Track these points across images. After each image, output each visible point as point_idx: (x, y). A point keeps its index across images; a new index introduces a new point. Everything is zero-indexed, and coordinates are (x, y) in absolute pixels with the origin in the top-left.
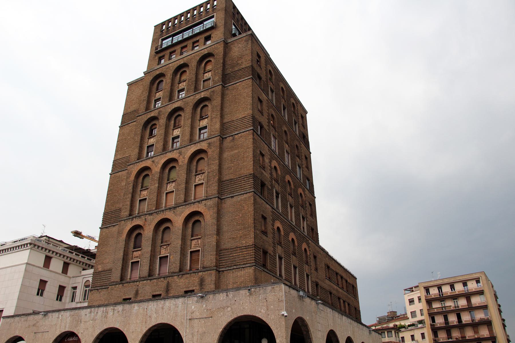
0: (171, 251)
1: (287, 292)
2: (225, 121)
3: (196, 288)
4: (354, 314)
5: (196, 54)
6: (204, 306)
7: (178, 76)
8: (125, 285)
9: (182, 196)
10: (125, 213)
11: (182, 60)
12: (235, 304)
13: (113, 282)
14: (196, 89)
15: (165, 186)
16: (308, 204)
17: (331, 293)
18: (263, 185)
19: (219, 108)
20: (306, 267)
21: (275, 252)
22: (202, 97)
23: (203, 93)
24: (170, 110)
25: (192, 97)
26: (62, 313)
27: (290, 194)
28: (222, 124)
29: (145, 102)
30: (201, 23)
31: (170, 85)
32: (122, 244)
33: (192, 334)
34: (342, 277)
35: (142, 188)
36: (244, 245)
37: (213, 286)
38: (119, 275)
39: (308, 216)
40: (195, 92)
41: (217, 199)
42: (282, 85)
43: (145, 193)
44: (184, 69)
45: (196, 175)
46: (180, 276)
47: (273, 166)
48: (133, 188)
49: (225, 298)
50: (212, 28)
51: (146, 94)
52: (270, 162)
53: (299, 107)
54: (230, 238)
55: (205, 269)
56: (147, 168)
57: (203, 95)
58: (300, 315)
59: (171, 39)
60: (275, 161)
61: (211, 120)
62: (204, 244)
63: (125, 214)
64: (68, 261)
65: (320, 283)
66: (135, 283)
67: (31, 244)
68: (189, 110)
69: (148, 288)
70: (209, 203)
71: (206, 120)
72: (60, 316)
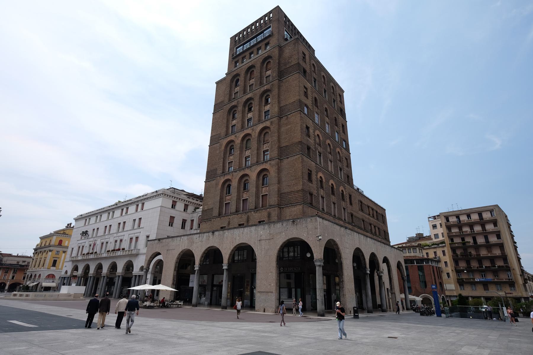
0: (250, 196)
2: (282, 105)
3: (266, 219)
4: (383, 236)
9: (255, 159)
10: (220, 171)
14: (261, 84)
16: (344, 158)
17: (363, 221)
18: (309, 148)
19: (277, 96)
21: (318, 193)
23: (265, 87)
25: (258, 90)
27: (330, 153)
28: (280, 108)
29: (228, 95)
30: (262, 32)
31: (243, 82)
32: (219, 192)
34: (373, 209)
37: (276, 218)
39: (345, 167)
42: (323, 74)
43: (231, 157)
47: (316, 134)
50: (270, 36)
51: (228, 90)
52: (314, 132)
53: (337, 88)
56: (249, 135)
57: (265, 88)
61: (272, 105)
62: (271, 190)
64: (187, 203)
65: (354, 214)
67: (162, 194)
68: (257, 99)
69: (236, 220)
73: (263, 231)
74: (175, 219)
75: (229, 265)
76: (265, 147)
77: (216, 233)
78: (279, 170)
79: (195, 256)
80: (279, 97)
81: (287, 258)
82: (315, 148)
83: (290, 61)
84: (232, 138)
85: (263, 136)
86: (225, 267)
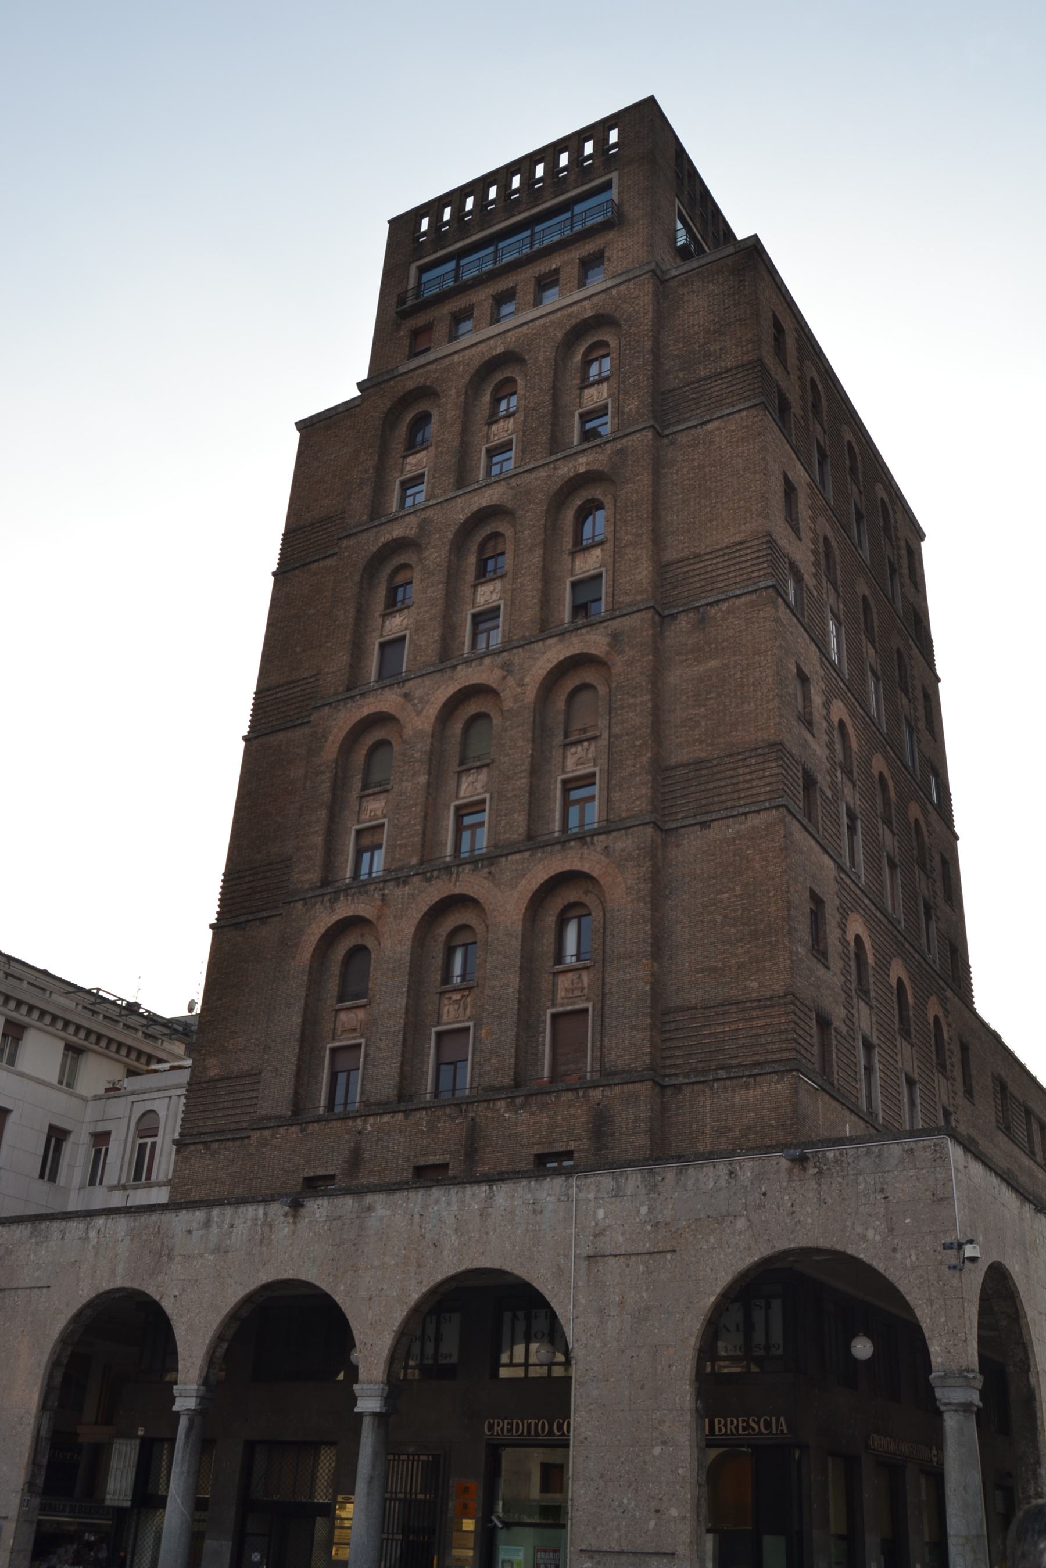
1: (961, 1168)
5: (552, 317)
6: (644, 1210)
7: (487, 398)
8: (310, 1128)
9: (520, 819)
11: (499, 341)
12: (761, 1206)
13: (268, 1118)
14: (556, 444)
15: (452, 783)
18: (809, 783)
20: (941, 1085)
21: (849, 1019)
22: (582, 470)
24: (462, 517)
25: (543, 473)
26: (100, 1221)
28: (661, 569)
29: (367, 490)
31: (457, 428)
33: (601, 1311)
35: (365, 787)
36: (754, 995)
37: (642, 1141)
38: (288, 1092)
40: (552, 454)
41: (650, 830)
43: (376, 806)
44: (508, 373)
45: (566, 746)
46: (518, 1101)
48: (334, 789)
49: (723, 1183)
50: (607, 226)
52: (827, 705)
53: (899, 516)
54: (702, 970)
55: (608, 1077)
57: (582, 464)
58: (995, 1258)
59: (452, 265)
60: (841, 704)
61: (617, 552)
63: (306, 877)
66: (350, 1123)
68: (532, 517)
69: (395, 1141)
70: (620, 845)
71: (597, 552)
72: (93, 1234)
73: (604, 1208)
74: (12, 1120)
75: (395, 1389)
76: (570, 762)
77: (318, 1208)
78: (658, 890)
79: (180, 1330)
80: (656, 515)
81: (519, 1372)
82: (833, 785)
83: (715, 347)
84: (388, 701)
85: (561, 704)
86: (369, 1403)
